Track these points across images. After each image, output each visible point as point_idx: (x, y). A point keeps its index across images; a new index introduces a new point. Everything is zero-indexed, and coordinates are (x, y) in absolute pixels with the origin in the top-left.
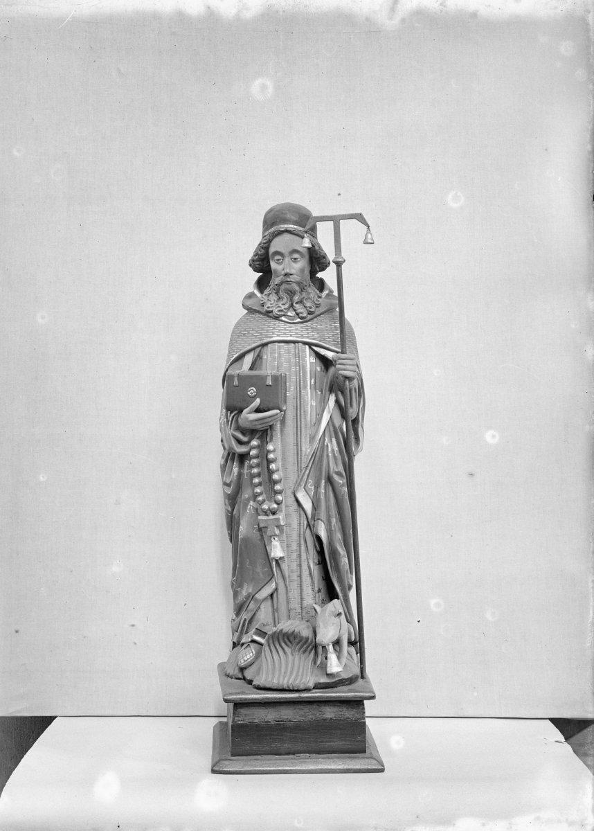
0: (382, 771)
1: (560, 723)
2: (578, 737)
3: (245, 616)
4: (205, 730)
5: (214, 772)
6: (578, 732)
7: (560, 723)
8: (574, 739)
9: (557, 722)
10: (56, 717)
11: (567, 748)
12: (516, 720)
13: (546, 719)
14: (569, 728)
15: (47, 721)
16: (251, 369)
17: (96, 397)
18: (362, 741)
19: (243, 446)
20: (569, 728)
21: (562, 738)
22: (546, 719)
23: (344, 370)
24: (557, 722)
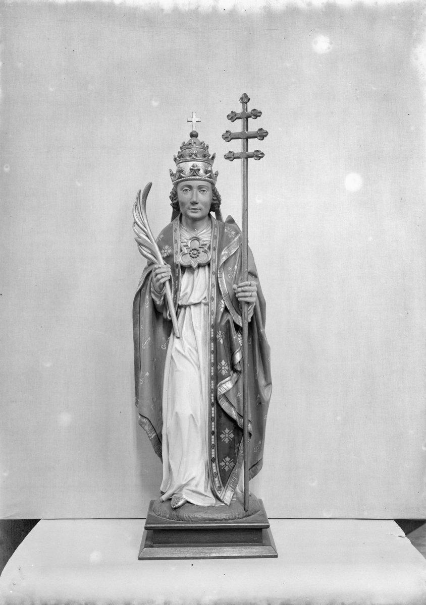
0: (276, 556)
1: (402, 523)
2: (416, 533)
3: (174, 413)
4: (139, 528)
5: (140, 559)
6: (415, 529)
7: (402, 523)
8: (410, 534)
9: (400, 522)
10: (40, 520)
11: (407, 541)
12: (368, 521)
13: (392, 519)
14: (408, 526)
15: (34, 522)
16: (176, 348)
17: (8, 125)
18: (30, 522)
19: (188, 184)
20: (408, 526)
21: (403, 534)
22: (392, 519)
23: (245, 297)
24: (400, 522)
